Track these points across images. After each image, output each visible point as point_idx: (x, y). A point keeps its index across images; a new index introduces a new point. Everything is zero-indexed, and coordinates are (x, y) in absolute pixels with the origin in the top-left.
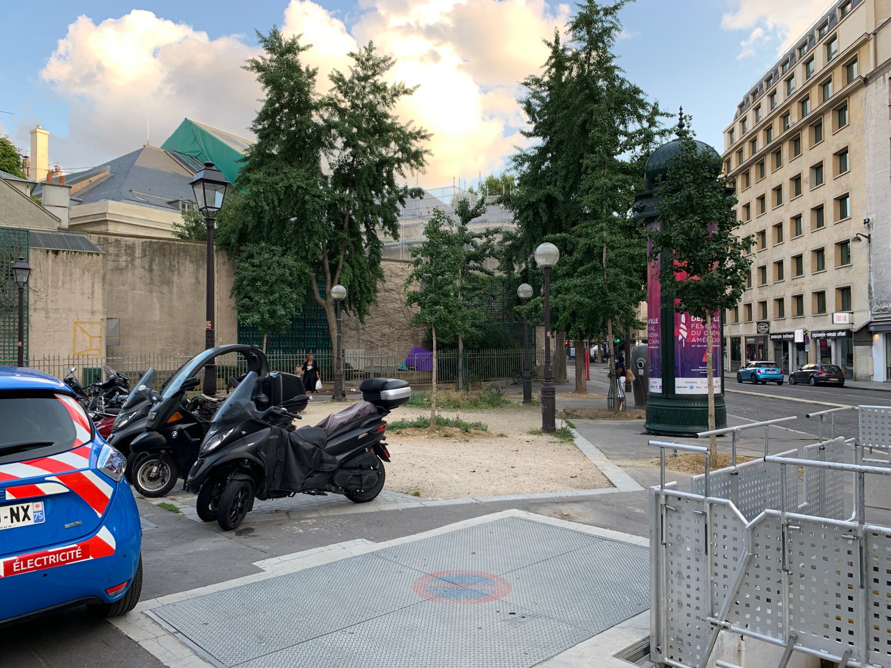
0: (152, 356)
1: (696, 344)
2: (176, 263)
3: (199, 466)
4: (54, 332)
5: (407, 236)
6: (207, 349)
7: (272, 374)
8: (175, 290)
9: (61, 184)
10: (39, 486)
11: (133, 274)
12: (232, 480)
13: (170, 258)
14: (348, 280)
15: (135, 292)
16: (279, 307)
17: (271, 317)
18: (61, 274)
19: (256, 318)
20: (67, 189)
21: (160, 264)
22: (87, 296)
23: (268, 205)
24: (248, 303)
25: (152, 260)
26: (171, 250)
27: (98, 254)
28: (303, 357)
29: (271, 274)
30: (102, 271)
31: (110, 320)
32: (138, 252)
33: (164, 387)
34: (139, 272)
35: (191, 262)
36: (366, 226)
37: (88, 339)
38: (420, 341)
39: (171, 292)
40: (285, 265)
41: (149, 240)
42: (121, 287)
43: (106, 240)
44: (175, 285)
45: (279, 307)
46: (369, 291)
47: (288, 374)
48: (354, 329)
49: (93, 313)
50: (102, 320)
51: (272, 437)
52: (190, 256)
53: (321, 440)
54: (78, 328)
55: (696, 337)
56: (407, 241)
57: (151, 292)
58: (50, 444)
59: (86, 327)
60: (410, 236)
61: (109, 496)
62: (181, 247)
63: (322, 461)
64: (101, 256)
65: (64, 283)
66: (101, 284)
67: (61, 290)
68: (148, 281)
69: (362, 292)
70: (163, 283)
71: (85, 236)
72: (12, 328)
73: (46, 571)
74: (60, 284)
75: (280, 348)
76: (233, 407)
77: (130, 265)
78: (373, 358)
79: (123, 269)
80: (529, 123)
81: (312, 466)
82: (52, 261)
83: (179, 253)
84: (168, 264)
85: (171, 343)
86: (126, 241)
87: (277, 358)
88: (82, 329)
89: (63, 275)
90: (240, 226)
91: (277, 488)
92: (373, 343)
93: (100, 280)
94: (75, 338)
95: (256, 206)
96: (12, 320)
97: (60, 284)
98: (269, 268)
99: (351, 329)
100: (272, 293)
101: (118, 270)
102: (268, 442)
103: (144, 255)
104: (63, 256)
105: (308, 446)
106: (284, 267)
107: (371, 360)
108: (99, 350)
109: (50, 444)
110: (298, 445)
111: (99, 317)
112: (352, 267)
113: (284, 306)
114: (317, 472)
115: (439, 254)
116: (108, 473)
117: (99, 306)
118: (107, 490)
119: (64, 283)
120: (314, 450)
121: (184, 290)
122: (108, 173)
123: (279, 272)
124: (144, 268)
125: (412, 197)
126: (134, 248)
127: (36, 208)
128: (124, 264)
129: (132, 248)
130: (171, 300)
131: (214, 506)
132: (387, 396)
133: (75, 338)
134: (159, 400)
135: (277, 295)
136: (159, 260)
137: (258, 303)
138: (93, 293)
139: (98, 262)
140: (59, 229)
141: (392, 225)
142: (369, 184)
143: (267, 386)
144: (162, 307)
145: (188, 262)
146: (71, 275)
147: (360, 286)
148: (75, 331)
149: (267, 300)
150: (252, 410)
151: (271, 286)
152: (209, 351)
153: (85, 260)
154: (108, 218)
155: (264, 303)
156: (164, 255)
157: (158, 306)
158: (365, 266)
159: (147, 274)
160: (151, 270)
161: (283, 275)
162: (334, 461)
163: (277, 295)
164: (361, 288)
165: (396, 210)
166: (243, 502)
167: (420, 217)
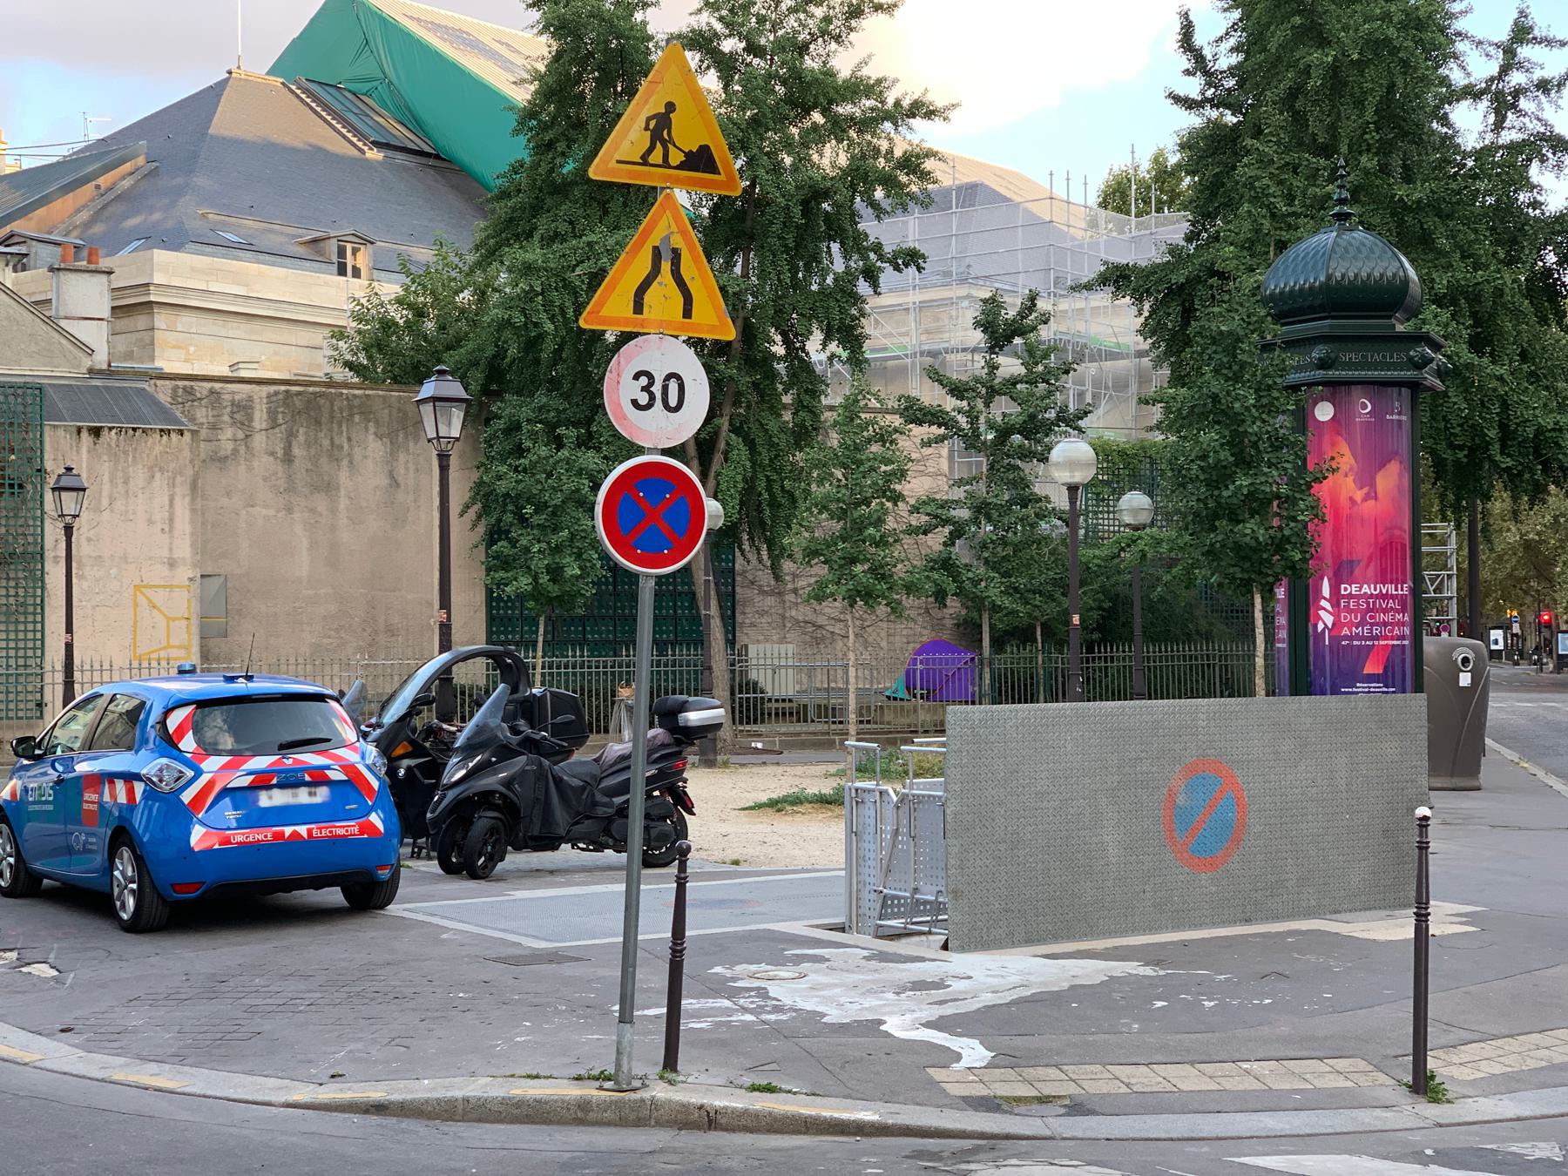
0: (292, 660)
1: (1351, 638)
2: (344, 439)
3: (440, 801)
4: (94, 608)
5: (928, 332)
6: (441, 653)
7: (534, 691)
8: (343, 502)
9: (92, 267)
10: (327, 772)
11: (250, 469)
12: (480, 817)
13: (331, 430)
14: (739, 478)
15: (255, 511)
16: (568, 559)
17: (554, 580)
18: (106, 478)
19: (524, 583)
20: (104, 278)
21: (308, 445)
22: (159, 526)
23: (552, 319)
24: (506, 551)
25: (291, 435)
26: (332, 411)
27: (181, 433)
28: (574, 667)
29: (553, 488)
30: (189, 472)
31: (206, 580)
32: (260, 418)
33: (384, 706)
34: (263, 463)
35: (379, 436)
36: (787, 342)
37: (162, 623)
38: (949, 623)
39: (334, 511)
40: (581, 469)
41: (283, 388)
42: (225, 501)
43: (189, 391)
44: (343, 493)
45: (568, 559)
46: (793, 500)
47: (562, 691)
48: (772, 593)
49: (172, 564)
50: (191, 579)
51: (528, 768)
52: (377, 422)
53: (594, 777)
54: (142, 600)
55: (1350, 625)
56: (926, 347)
57: (290, 510)
58: (329, 740)
59: (159, 597)
60: (939, 331)
61: (376, 788)
62: (356, 402)
63: (595, 804)
64: (187, 436)
65: (112, 500)
66: (187, 499)
67: (106, 514)
68: (282, 483)
69: (774, 504)
70: (316, 489)
71: (145, 386)
72: (12, 600)
73: (335, 840)
74: (105, 502)
75: (582, 643)
76: (480, 729)
77: (242, 449)
78: (814, 668)
79: (226, 457)
80: (1187, 72)
81: (581, 809)
82: (89, 452)
83: (352, 415)
84: (326, 442)
85: (337, 631)
86: (234, 393)
87: (574, 667)
88: (150, 601)
89: (111, 481)
90: (490, 351)
91: (536, 833)
92: (820, 627)
93: (186, 490)
94: (136, 622)
95: (526, 324)
96: (12, 584)
97: (105, 502)
98: (550, 475)
99: (762, 592)
100: (555, 530)
101: (220, 460)
102: (523, 772)
103: (274, 425)
104: (109, 438)
105: (576, 782)
106: (579, 473)
107: (811, 671)
108: (187, 648)
109: (329, 740)
110: (561, 780)
111: (185, 573)
112: (751, 445)
113: (579, 556)
114: (588, 817)
115: (859, 463)
116: (373, 768)
117: (184, 549)
118: (375, 784)
119: (112, 500)
120: (583, 789)
121: (364, 504)
122: (141, 161)
123: (568, 486)
124: (273, 454)
125: (897, 268)
126: (251, 408)
127: (44, 327)
128: (229, 446)
129: (245, 407)
130: (333, 528)
131: (459, 856)
132: (687, 720)
133: (136, 622)
134: (379, 725)
135: (565, 533)
136: (306, 433)
137: (527, 550)
138: (171, 520)
139: (181, 450)
140: (90, 371)
141: (848, 334)
142: (786, 246)
143: (528, 709)
144: (313, 546)
145: (371, 438)
146: (126, 482)
147: (769, 489)
148: (136, 605)
149: (544, 545)
150: (505, 733)
151: (554, 513)
152: (446, 656)
153: (155, 445)
154: (152, 298)
155: (539, 551)
156: (318, 423)
157: (305, 543)
158: (782, 440)
159: (280, 468)
160: (288, 459)
161: (578, 490)
162: (610, 805)
163: (565, 533)
164: (771, 494)
165: (857, 299)
166: (493, 847)
167: (963, 281)
